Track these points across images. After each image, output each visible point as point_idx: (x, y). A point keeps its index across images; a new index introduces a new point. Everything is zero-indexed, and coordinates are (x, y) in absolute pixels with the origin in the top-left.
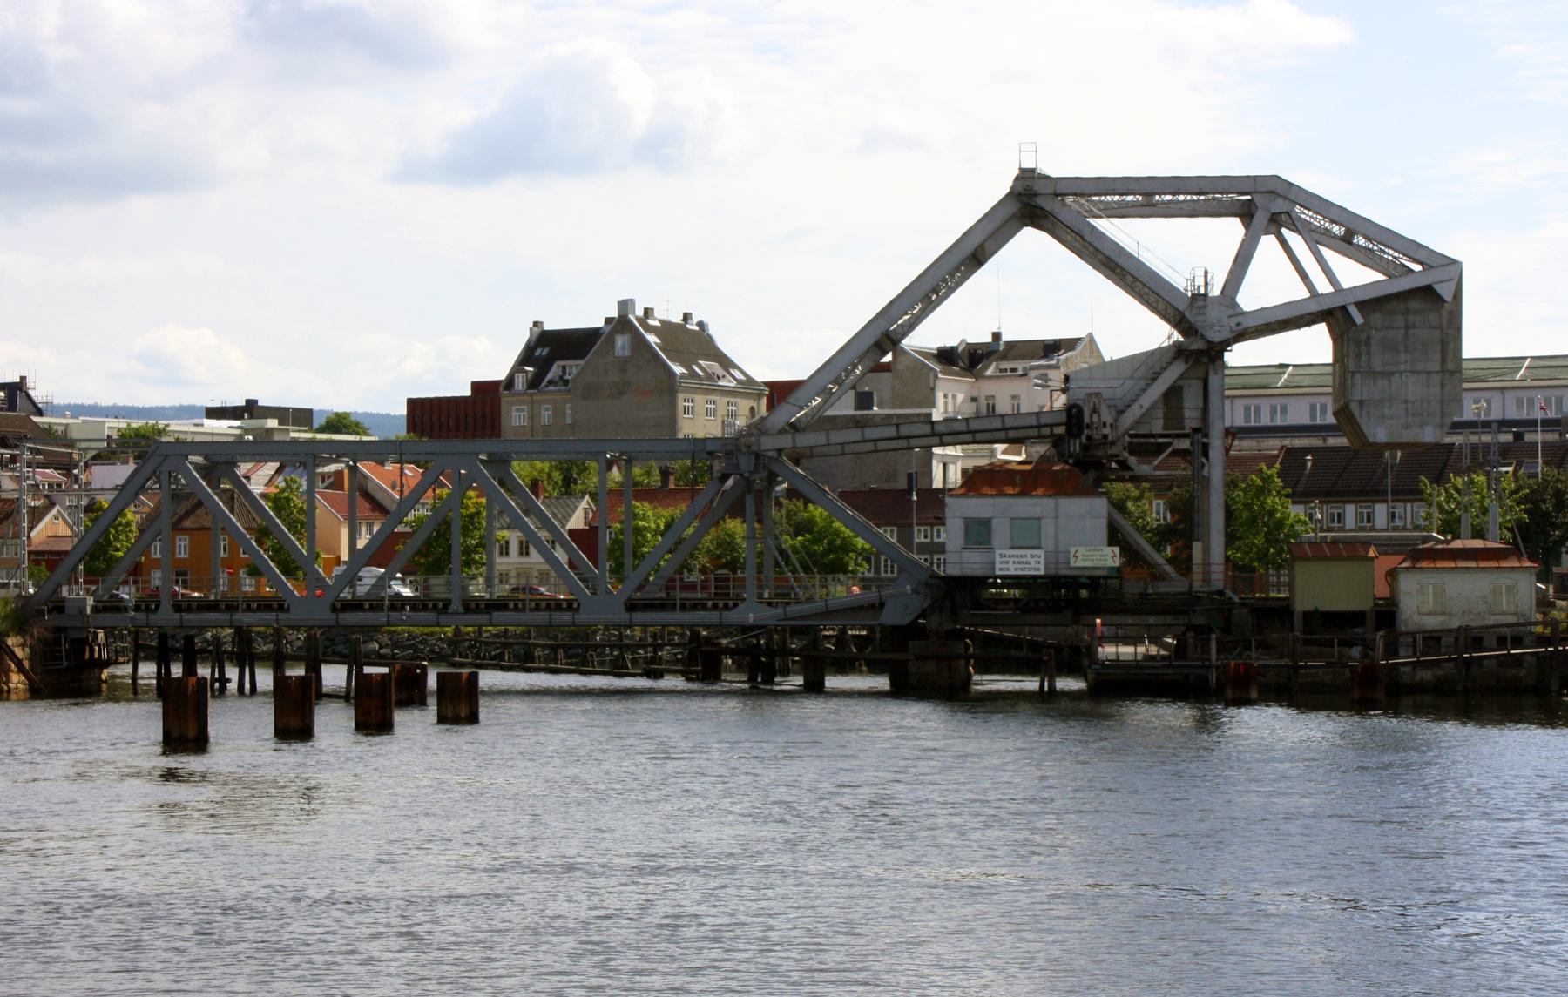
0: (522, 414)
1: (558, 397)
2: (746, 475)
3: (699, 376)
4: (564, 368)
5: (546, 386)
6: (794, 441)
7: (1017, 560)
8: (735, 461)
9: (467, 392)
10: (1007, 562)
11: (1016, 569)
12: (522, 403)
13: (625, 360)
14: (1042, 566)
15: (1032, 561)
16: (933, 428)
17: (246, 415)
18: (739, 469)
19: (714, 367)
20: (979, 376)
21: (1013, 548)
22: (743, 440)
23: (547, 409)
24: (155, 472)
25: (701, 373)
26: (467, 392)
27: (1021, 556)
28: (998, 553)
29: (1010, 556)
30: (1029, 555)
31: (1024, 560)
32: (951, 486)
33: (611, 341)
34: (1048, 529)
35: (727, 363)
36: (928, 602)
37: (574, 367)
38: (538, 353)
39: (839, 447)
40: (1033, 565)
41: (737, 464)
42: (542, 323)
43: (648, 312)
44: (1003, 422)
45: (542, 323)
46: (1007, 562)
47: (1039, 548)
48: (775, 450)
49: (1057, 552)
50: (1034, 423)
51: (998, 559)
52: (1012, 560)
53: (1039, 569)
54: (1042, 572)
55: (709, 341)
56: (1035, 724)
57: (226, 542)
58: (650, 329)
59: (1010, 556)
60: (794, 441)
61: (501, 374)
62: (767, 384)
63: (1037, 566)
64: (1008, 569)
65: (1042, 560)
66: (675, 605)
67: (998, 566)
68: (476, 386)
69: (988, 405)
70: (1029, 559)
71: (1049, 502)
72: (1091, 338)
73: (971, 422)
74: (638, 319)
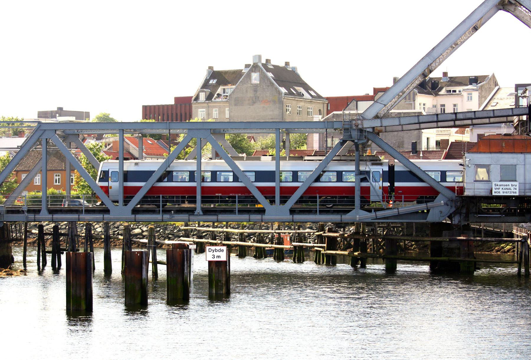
0: (203, 113)
1: (221, 104)
2: (356, 141)
3: (294, 94)
4: (224, 90)
5: (215, 99)
6: (381, 123)
7: (504, 187)
8: (349, 134)
9: (172, 102)
10: (499, 189)
11: (503, 192)
12: (203, 108)
13: (256, 86)
14: (517, 191)
15: (512, 188)
16: (456, 116)
17: (57, 115)
18: (352, 138)
19: (301, 90)
20: (437, 94)
21: (501, 181)
22: (354, 122)
23: (216, 111)
24: (39, 139)
25: (295, 92)
26: (172, 102)
27: (506, 185)
28: (494, 183)
29: (500, 185)
30: (510, 185)
31: (507, 187)
32: (431, 150)
33: (249, 76)
34: (520, 171)
35: (307, 88)
36: (453, 209)
37: (230, 89)
38: (211, 82)
39: (404, 128)
40: (513, 191)
41: (351, 135)
42: (213, 67)
43: (268, 61)
44: (475, 115)
45: (213, 67)
46: (499, 189)
47: (516, 181)
48: (371, 128)
49: (525, 183)
50: (435, 119)
51: (494, 187)
52: (501, 187)
53: (516, 193)
54: (517, 194)
55: (298, 76)
56: (420, 263)
57: (60, 177)
58: (268, 70)
59: (500, 185)
60: (381, 123)
61: (192, 93)
62: (328, 99)
63: (515, 191)
64: (499, 192)
65: (517, 187)
66: (316, 211)
67: (494, 191)
68: (177, 99)
69: (441, 109)
70: (510, 187)
71: (521, 156)
72: (493, 76)
73: (439, 116)
74: (263, 64)
